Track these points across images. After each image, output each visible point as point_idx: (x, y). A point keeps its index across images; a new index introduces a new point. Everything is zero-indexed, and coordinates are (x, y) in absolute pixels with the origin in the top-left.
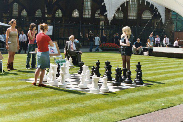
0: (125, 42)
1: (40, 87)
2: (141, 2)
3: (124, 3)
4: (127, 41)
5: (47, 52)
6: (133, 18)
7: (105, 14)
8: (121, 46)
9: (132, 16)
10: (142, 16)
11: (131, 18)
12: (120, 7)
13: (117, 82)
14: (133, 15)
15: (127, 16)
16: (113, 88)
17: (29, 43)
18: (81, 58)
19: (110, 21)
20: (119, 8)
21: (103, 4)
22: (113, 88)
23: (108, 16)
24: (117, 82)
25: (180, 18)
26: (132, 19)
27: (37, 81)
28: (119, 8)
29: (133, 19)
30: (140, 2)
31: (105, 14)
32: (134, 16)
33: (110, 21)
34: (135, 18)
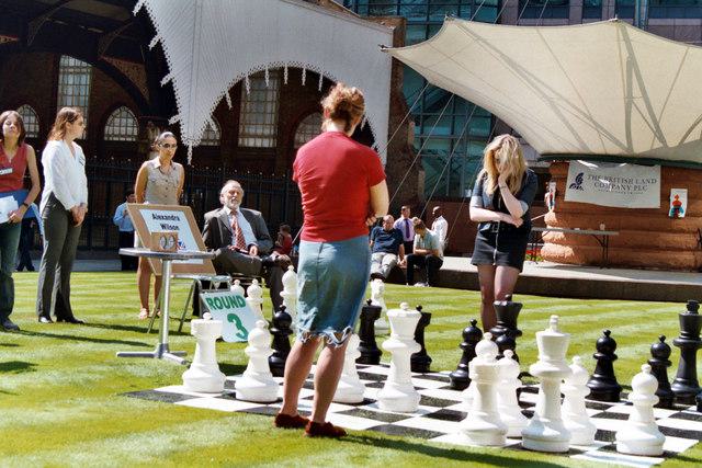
0: (497, 204)
1: (282, 431)
2: (304, 80)
3: (283, 69)
4: (507, 197)
5: (353, 240)
6: (259, 143)
7: (172, 121)
8: (474, 224)
9: (255, 136)
10: (296, 138)
11: (251, 143)
12: (228, 96)
13: (603, 385)
14: (258, 135)
15: (236, 135)
16: (457, 402)
17: (300, 186)
18: (71, 293)
19: (190, 150)
20: (224, 98)
21: (164, 82)
22: (457, 402)
23: (184, 130)
24: (603, 385)
25: (430, 151)
26: (255, 149)
27: (333, 407)
28: (224, 98)
29: (262, 149)
30: (301, 78)
31: (172, 121)
32: (262, 136)
33: (190, 150)
34: (267, 143)
